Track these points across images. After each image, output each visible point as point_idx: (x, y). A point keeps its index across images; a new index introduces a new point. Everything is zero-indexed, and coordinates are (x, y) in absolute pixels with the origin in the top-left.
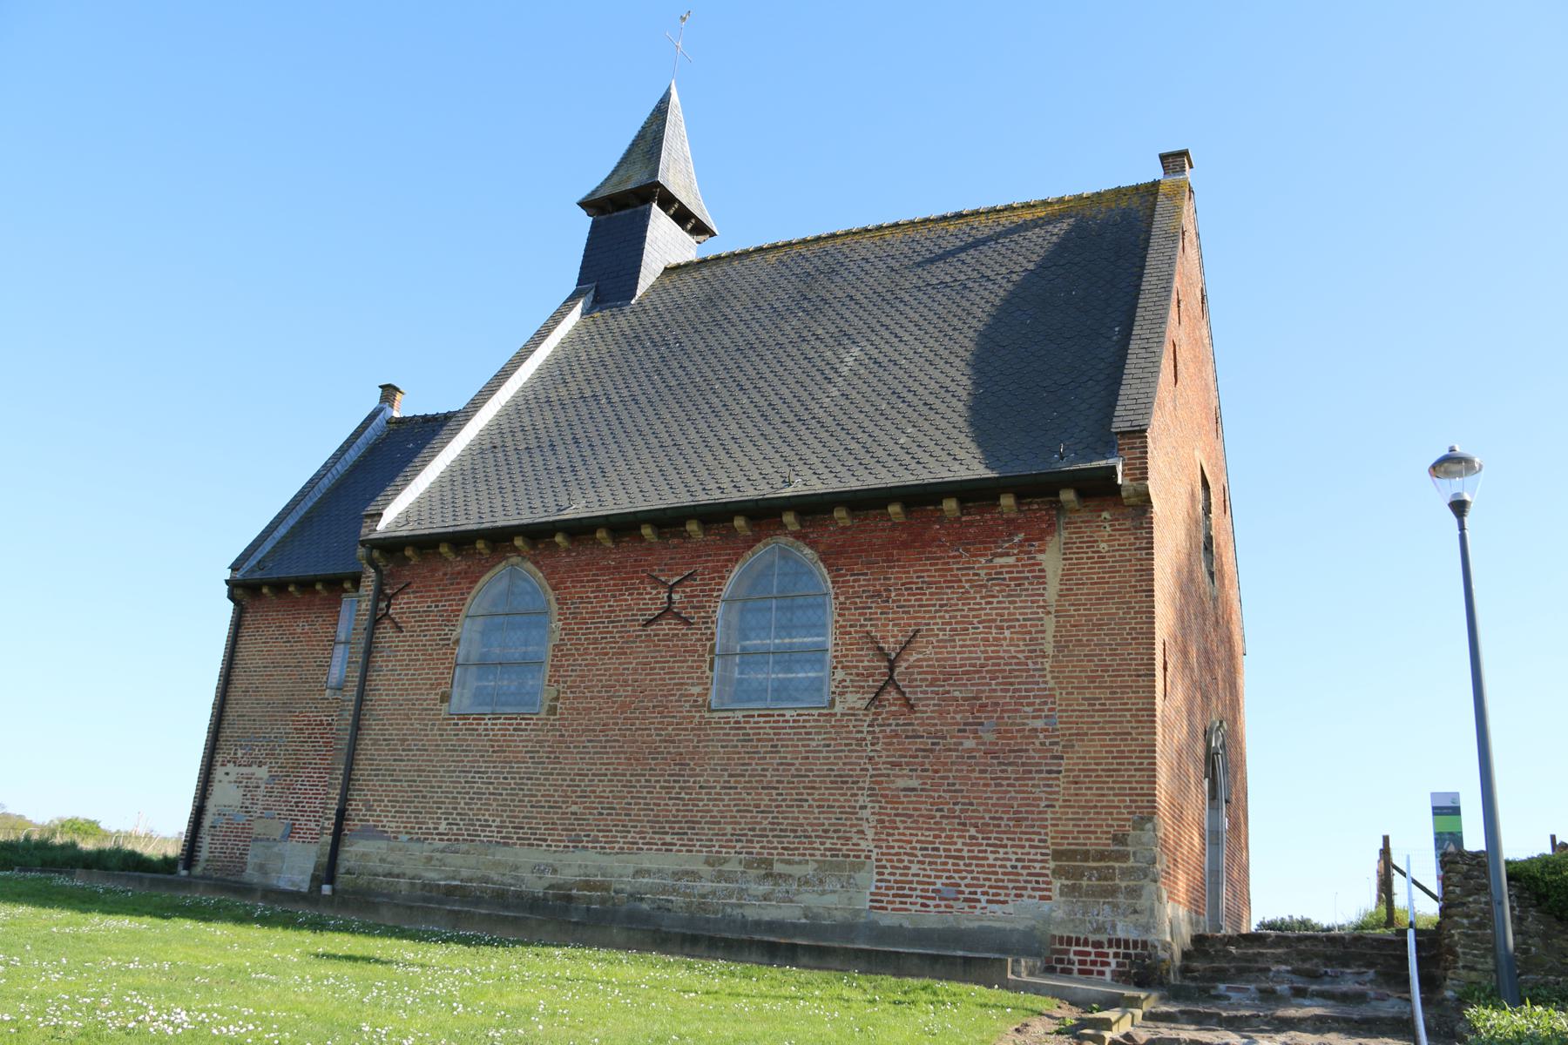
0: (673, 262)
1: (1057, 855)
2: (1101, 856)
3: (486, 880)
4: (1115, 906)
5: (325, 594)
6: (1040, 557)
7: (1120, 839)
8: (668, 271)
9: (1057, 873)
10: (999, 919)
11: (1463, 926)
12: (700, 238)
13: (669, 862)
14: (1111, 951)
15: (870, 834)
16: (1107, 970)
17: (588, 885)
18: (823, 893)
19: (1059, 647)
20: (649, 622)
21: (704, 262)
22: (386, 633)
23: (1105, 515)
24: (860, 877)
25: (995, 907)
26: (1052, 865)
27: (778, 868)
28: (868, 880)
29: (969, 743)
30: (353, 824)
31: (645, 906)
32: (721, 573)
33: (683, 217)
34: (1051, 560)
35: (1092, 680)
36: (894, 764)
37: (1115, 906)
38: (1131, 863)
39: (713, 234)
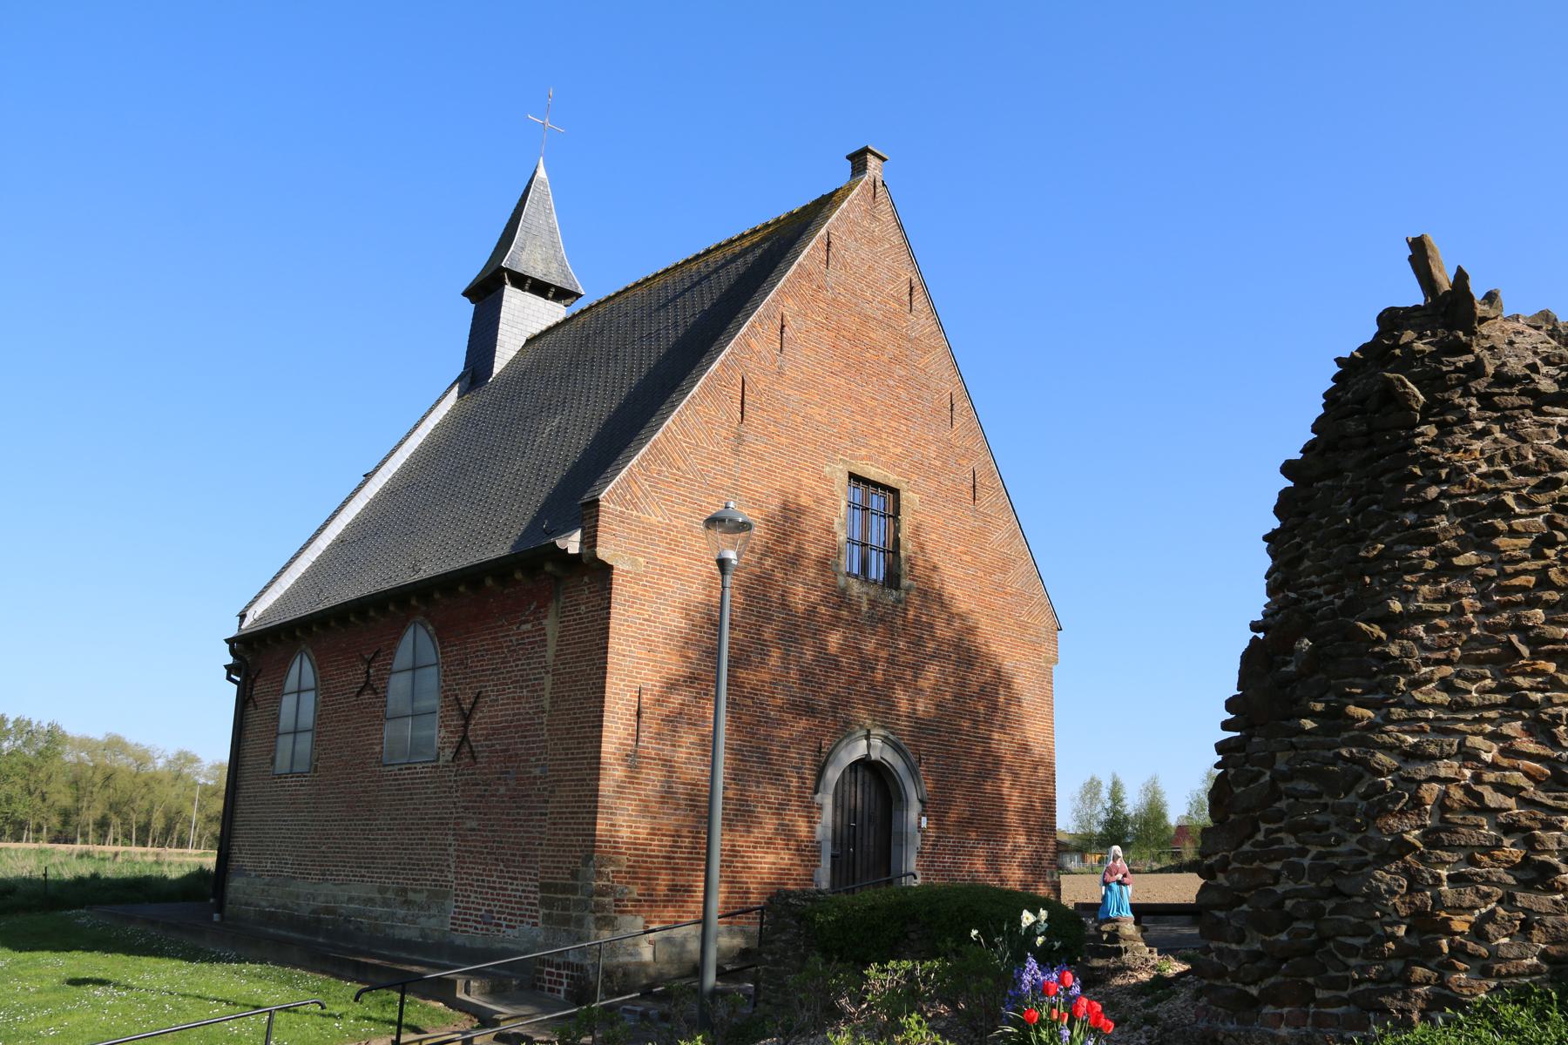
0: (536, 329)
1: (544, 887)
2: (565, 889)
3: (285, 907)
5: (424, 608)
6: (545, 622)
7: (574, 875)
8: (529, 342)
9: (545, 903)
10: (510, 942)
11: (767, 962)
14: (564, 972)
16: (562, 988)
17: (328, 910)
18: (430, 917)
19: (553, 703)
20: (359, 694)
21: (566, 321)
23: (586, 579)
26: (539, 896)
27: (411, 896)
28: (450, 904)
29: (502, 790)
32: (391, 652)
33: (540, 288)
36: (466, 808)
38: (579, 896)
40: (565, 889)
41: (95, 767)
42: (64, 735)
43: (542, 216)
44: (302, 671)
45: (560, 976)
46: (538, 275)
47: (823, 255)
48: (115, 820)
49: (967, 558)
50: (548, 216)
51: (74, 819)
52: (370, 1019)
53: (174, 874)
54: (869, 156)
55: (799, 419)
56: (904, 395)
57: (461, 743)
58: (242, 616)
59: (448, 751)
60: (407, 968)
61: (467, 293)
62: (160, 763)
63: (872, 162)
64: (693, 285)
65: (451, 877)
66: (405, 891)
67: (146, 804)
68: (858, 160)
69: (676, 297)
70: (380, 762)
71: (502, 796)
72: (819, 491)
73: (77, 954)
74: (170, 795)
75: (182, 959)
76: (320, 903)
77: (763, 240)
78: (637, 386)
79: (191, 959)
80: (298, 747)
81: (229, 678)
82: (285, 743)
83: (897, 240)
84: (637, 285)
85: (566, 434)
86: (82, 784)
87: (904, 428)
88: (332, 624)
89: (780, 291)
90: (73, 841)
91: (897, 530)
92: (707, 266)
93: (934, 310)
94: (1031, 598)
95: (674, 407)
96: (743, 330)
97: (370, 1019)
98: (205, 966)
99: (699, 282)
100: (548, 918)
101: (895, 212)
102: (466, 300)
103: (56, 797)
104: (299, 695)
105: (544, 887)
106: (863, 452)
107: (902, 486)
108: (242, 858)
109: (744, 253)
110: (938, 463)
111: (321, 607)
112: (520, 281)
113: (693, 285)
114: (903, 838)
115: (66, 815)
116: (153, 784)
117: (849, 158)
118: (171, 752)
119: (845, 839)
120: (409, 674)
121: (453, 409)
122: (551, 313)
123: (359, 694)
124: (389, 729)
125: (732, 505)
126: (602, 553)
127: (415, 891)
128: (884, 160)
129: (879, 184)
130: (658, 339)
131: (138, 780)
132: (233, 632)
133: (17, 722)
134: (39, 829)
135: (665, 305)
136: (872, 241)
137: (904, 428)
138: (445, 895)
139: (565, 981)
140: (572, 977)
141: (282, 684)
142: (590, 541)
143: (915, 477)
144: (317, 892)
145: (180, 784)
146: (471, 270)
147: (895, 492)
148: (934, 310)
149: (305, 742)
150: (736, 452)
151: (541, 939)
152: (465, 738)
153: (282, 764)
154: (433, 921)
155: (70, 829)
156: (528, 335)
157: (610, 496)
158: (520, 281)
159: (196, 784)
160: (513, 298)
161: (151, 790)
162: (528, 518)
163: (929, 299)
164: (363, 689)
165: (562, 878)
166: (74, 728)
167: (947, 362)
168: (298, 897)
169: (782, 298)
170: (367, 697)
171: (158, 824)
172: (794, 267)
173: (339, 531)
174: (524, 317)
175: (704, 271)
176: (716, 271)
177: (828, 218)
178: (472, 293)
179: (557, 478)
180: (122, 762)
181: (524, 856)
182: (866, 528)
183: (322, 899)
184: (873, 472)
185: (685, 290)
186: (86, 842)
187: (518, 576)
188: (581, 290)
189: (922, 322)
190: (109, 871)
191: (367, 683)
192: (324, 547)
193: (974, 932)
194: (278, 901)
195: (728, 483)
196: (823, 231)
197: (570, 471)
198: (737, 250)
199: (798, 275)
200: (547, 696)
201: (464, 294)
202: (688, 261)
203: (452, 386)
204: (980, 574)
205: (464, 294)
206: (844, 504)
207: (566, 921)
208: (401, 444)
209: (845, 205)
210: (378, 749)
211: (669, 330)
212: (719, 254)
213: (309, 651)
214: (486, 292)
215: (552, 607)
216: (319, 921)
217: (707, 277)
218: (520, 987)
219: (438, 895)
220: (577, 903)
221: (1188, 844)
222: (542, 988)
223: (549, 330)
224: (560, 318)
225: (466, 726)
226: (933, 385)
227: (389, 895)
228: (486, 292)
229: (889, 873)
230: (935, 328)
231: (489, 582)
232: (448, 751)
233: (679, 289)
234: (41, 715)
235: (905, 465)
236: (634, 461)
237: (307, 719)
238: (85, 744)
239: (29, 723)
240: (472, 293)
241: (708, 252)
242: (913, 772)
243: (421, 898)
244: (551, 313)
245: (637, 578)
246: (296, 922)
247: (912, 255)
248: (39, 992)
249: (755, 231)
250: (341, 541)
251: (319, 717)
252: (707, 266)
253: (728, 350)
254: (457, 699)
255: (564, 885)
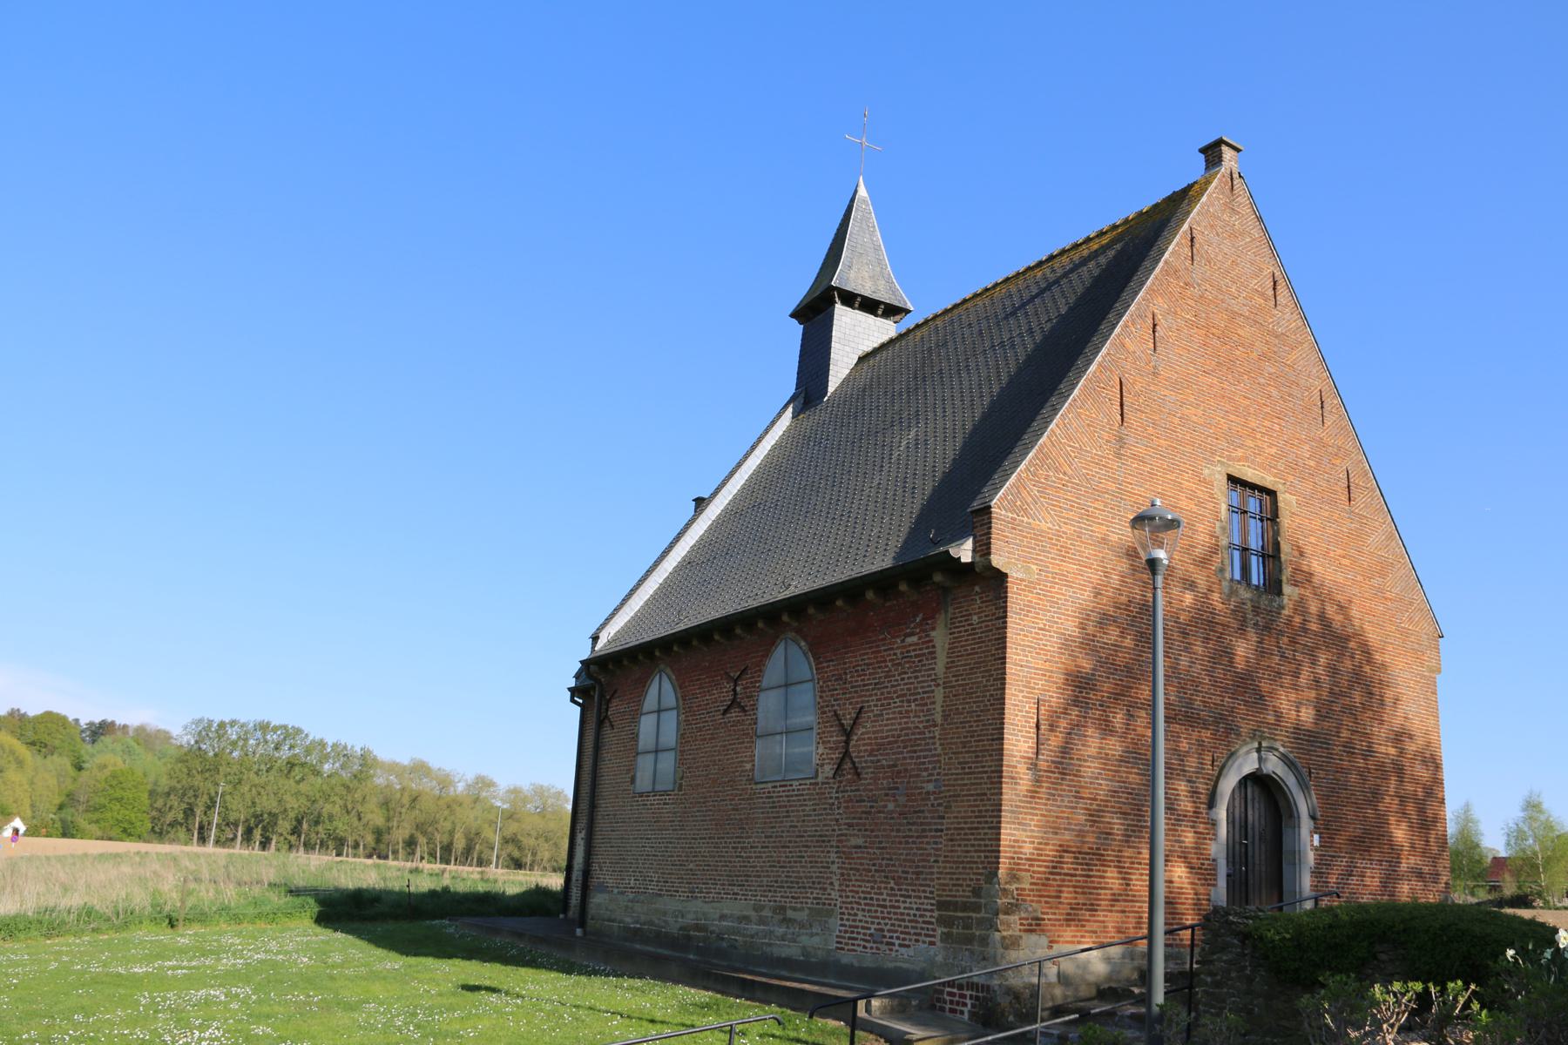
0: (869, 345)
1: (942, 905)
2: (965, 907)
3: (651, 923)
4: (972, 952)
5: (795, 624)
6: (933, 634)
7: (977, 892)
8: (861, 359)
9: (942, 921)
10: (905, 961)
11: (1206, 984)
12: (897, 318)
13: (730, 907)
14: (968, 993)
15: (836, 884)
16: (966, 1010)
17: (698, 928)
18: (812, 935)
19: (945, 717)
20: (725, 712)
21: (901, 337)
22: (607, 730)
23: (977, 588)
24: (831, 920)
25: (903, 950)
26: (936, 914)
27: (790, 914)
28: (835, 923)
29: (891, 806)
30: (594, 882)
31: (725, 944)
32: (760, 668)
33: (869, 306)
34: (940, 637)
35: (964, 744)
36: (850, 825)
37: (972, 952)
38: (982, 915)
39: (907, 311)
40: (965, 907)
41: (403, 789)
42: (375, 759)
43: (865, 235)
44: (661, 690)
45: (963, 996)
46: (867, 292)
47: (1187, 251)
48: (422, 840)
49: (1345, 562)
50: (872, 234)
51: (386, 837)
52: (773, 1036)
53: (512, 890)
54: (1224, 148)
55: (1176, 421)
56: (1275, 393)
57: (842, 759)
58: (595, 639)
59: (827, 768)
60: (788, 984)
61: (797, 314)
62: (461, 787)
63: (1227, 153)
64: (1042, 291)
65: (834, 895)
66: (783, 909)
67: (448, 825)
68: (1212, 153)
69: (1023, 305)
70: (751, 780)
71: (892, 812)
72: (1199, 494)
73: (457, 962)
74: (471, 817)
75: (558, 970)
76: (689, 920)
77: (1113, 242)
78: (999, 395)
79: (569, 972)
80: (659, 766)
81: (573, 700)
82: (645, 765)
83: (1257, 233)
84: (976, 296)
85: (929, 446)
86: (392, 805)
87: (1277, 427)
88: (695, 643)
89: (1150, 289)
90: (386, 857)
91: (1277, 533)
92: (1053, 271)
93: (1298, 304)
94: (1411, 604)
95: (1055, 411)
96: (1117, 330)
97: (773, 1036)
98: (583, 979)
99: (1048, 288)
100: (946, 937)
101: (1253, 203)
102: (794, 321)
103: (369, 816)
104: (659, 714)
105: (942, 905)
106: (1240, 453)
107: (1279, 488)
108: (604, 874)
109: (1095, 255)
110: (1312, 463)
111: (682, 627)
112: (849, 299)
113: (1042, 291)
114: (1296, 855)
115: (379, 834)
116: (454, 806)
117: (1202, 151)
118: (470, 777)
119: (1238, 854)
120: (782, 690)
121: (789, 429)
122: (879, 330)
123: (725, 712)
124: (760, 748)
125: (1158, 503)
126: (997, 561)
127: (795, 909)
128: (1238, 150)
129: (1236, 176)
130: (1013, 346)
131: (441, 802)
132: (586, 655)
133: (335, 746)
134: (356, 846)
135: (1013, 313)
136: (1234, 235)
137: (1277, 427)
138: (830, 913)
139: (968, 1001)
140: (977, 998)
141: (640, 703)
142: (983, 548)
143: (1291, 478)
144: (680, 910)
145: (478, 806)
146: (799, 289)
147: (1272, 494)
148: (1298, 304)
149: (667, 762)
150: (1118, 455)
151: (939, 958)
152: (846, 754)
153: (643, 782)
154: (816, 939)
155: (382, 846)
156: (860, 353)
157: (1001, 503)
158: (849, 299)
159: (492, 807)
160: (845, 319)
161: (452, 812)
162: (905, 530)
163: (1293, 293)
164: (729, 707)
165: (962, 895)
166: (385, 752)
167: (1314, 357)
168: (665, 914)
169: (1152, 298)
170: (734, 714)
171: (460, 844)
172: (1161, 264)
173: (683, 554)
174: (854, 335)
175: (1051, 277)
176: (1065, 275)
177: (1189, 213)
178: (800, 314)
179: (928, 490)
180: (427, 786)
181: (917, 873)
182: (1244, 533)
183: (691, 916)
184: (1250, 474)
185: (1032, 298)
186: (396, 859)
187: (903, 587)
188: (910, 306)
189: (1287, 316)
190: (461, 887)
191: (733, 701)
192: (670, 569)
193: (1510, 953)
194: (643, 918)
195: (1112, 487)
196: (1186, 226)
197: (942, 481)
198: (1085, 253)
199: (1166, 272)
200: (939, 709)
201: (792, 316)
202: (1029, 269)
203: (786, 407)
204: (1359, 578)
205: (792, 316)
206: (1224, 507)
207: (969, 940)
208: (739, 465)
209: (1204, 199)
210: (748, 766)
211: (1024, 339)
212: (1065, 259)
213: (668, 670)
214: (815, 312)
215: (941, 620)
216: (689, 938)
217: (1057, 281)
218: (919, 1008)
219: (821, 913)
220: (980, 922)
221: (1507, 877)
222: (942, 1009)
223: (883, 347)
224: (885, 338)
225: (847, 742)
226: (1302, 382)
227: (767, 913)
228: (815, 312)
229: (1281, 900)
230: (1300, 323)
231: (870, 595)
232: (827, 768)
233: (1026, 296)
234: (355, 742)
235: (1281, 466)
236: (1022, 466)
237: (670, 735)
238: (393, 768)
239: (345, 747)
240: (800, 314)
241: (1051, 258)
242: (1304, 786)
243: (803, 916)
244: (879, 330)
245: (1031, 587)
246: (661, 938)
247: (1272, 248)
248: (440, 995)
249: (1101, 234)
250: (687, 563)
251: (682, 736)
252: (1053, 271)
253: (1104, 351)
254: (836, 714)
255: (964, 903)
